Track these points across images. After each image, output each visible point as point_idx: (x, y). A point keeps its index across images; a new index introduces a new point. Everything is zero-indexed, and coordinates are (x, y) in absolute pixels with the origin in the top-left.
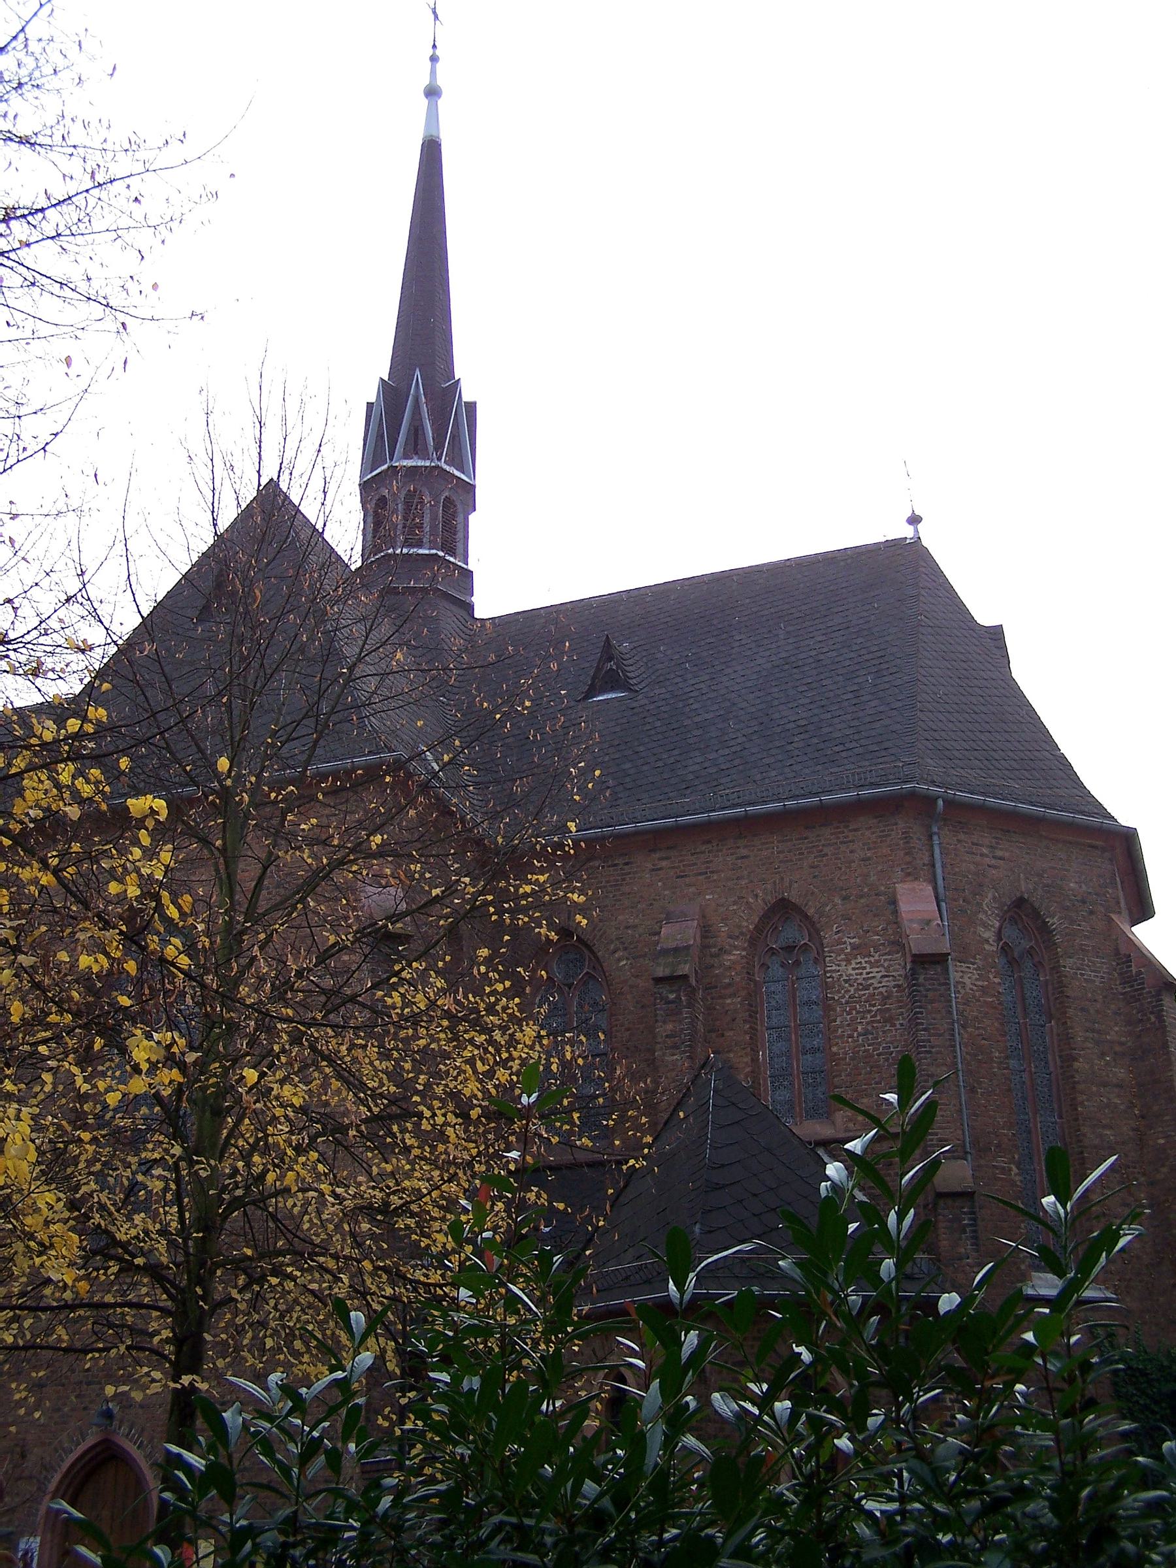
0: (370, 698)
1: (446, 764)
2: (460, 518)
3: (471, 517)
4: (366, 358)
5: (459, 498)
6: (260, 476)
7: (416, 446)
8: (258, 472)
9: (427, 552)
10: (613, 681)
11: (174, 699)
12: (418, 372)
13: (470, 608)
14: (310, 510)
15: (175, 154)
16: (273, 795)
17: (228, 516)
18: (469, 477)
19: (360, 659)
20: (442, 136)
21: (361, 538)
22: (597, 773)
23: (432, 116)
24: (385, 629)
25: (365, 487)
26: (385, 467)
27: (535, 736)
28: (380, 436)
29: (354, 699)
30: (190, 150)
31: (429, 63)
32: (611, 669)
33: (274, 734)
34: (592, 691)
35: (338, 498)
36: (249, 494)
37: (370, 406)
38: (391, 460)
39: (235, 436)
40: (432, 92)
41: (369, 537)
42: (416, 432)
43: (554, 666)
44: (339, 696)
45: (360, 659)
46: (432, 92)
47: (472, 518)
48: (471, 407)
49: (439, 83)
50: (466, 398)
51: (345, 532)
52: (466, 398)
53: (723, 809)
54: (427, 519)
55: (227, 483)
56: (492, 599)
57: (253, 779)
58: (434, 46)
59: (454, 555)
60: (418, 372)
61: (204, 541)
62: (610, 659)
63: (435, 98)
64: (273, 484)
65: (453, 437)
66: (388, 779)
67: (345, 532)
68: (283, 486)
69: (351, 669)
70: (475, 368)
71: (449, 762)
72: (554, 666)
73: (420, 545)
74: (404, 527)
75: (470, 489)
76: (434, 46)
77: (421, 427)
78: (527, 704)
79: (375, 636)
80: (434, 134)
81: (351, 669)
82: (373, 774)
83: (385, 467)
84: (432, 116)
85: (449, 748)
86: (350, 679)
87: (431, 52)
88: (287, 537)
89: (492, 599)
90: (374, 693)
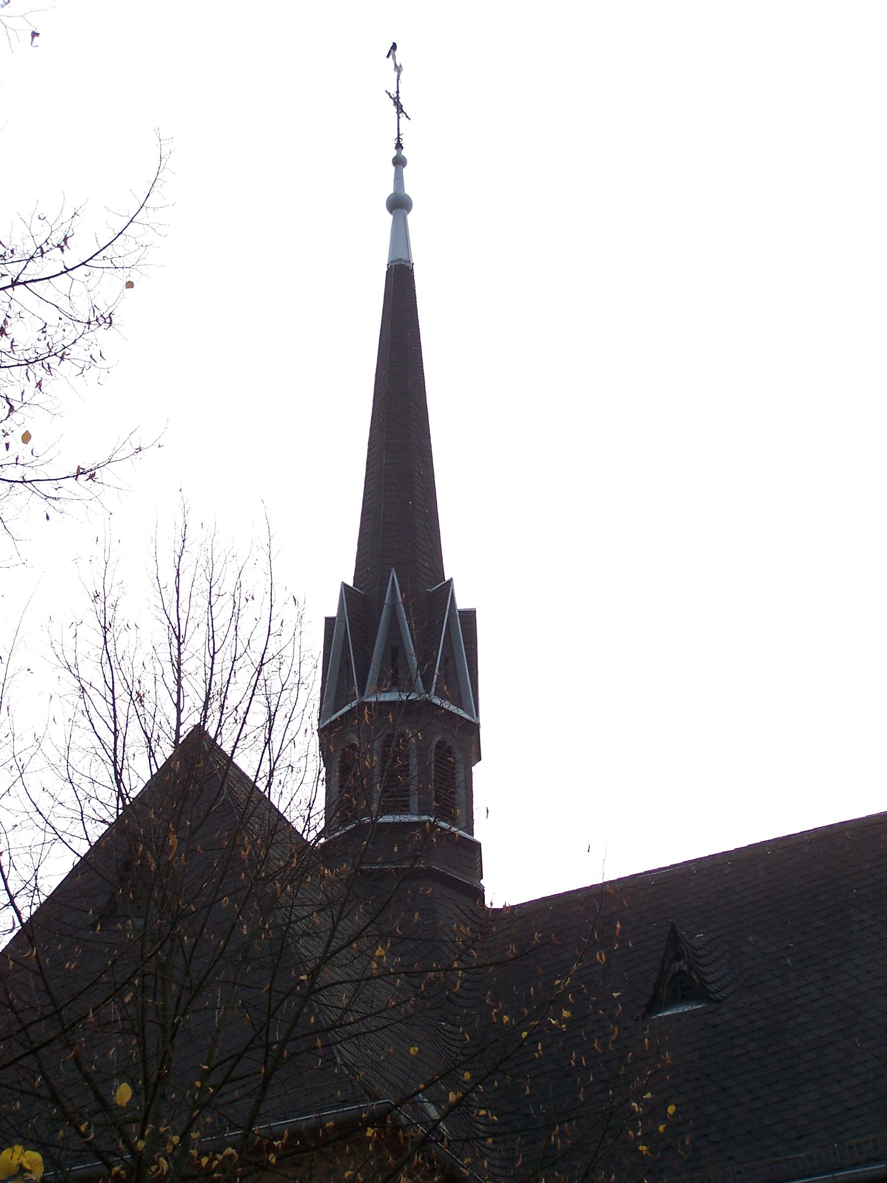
0: (341, 1017)
1: (452, 1107)
2: (460, 768)
3: (474, 769)
4: (323, 560)
5: (457, 743)
6: (179, 711)
7: (395, 676)
8: (177, 705)
9: (415, 819)
10: (684, 988)
11: (63, 1025)
12: (393, 574)
13: (479, 893)
14: (247, 761)
15: (52, 263)
16: (205, 1160)
17: (139, 775)
18: (469, 712)
19: (326, 959)
20: (414, 259)
21: (322, 790)
22: (671, 1109)
23: (400, 236)
24: (357, 919)
25: (324, 732)
26: (354, 704)
27: (578, 1062)
28: (345, 663)
29: (317, 1021)
30: (71, 258)
31: (392, 169)
32: (681, 971)
33: (206, 1074)
34: (655, 1004)
35: (288, 737)
36: (165, 751)
37: (329, 622)
38: (362, 693)
39: (143, 646)
40: (399, 204)
41: (335, 789)
42: (395, 653)
43: (601, 957)
44: (298, 1015)
45: (326, 959)
46: (399, 204)
47: (477, 770)
48: (469, 617)
49: (408, 191)
50: (462, 603)
51: (300, 793)
52: (462, 603)
53: (855, 1165)
54: (414, 761)
55: (134, 724)
56: (508, 882)
57: (176, 1139)
58: (399, 146)
59: (453, 821)
60: (393, 574)
61: (105, 809)
62: (678, 957)
63: (401, 166)
64: (199, 730)
65: (446, 659)
66: (370, 1132)
67: (300, 793)
68: (211, 729)
69: (314, 974)
70: (472, 563)
71: (459, 1103)
72: (601, 957)
73: (404, 808)
74: (383, 772)
75: (475, 728)
76: (399, 146)
77: (403, 654)
78: (566, 1014)
79: (347, 927)
80: (405, 257)
81: (314, 974)
82: (349, 1130)
83: (354, 704)
84: (400, 236)
85: (456, 1084)
86: (312, 990)
87: (394, 153)
88: (219, 795)
89: (508, 882)
90: (346, 1010)
